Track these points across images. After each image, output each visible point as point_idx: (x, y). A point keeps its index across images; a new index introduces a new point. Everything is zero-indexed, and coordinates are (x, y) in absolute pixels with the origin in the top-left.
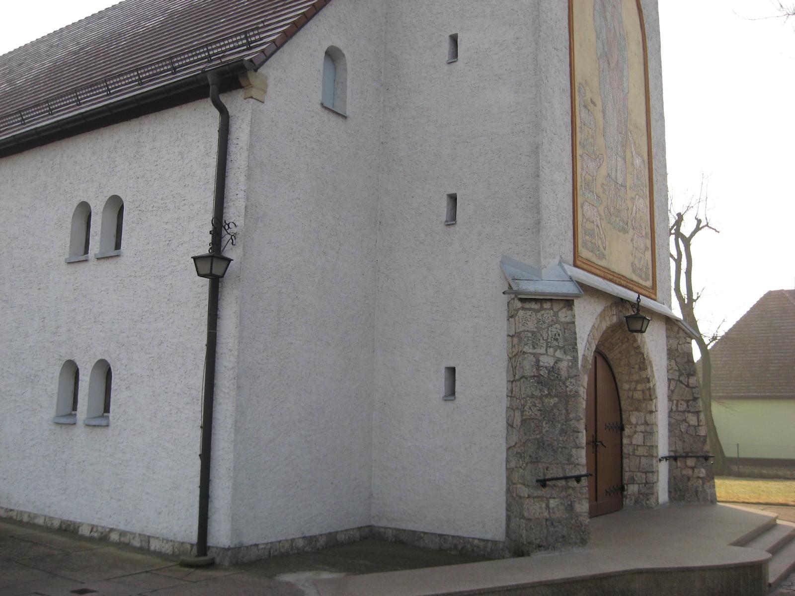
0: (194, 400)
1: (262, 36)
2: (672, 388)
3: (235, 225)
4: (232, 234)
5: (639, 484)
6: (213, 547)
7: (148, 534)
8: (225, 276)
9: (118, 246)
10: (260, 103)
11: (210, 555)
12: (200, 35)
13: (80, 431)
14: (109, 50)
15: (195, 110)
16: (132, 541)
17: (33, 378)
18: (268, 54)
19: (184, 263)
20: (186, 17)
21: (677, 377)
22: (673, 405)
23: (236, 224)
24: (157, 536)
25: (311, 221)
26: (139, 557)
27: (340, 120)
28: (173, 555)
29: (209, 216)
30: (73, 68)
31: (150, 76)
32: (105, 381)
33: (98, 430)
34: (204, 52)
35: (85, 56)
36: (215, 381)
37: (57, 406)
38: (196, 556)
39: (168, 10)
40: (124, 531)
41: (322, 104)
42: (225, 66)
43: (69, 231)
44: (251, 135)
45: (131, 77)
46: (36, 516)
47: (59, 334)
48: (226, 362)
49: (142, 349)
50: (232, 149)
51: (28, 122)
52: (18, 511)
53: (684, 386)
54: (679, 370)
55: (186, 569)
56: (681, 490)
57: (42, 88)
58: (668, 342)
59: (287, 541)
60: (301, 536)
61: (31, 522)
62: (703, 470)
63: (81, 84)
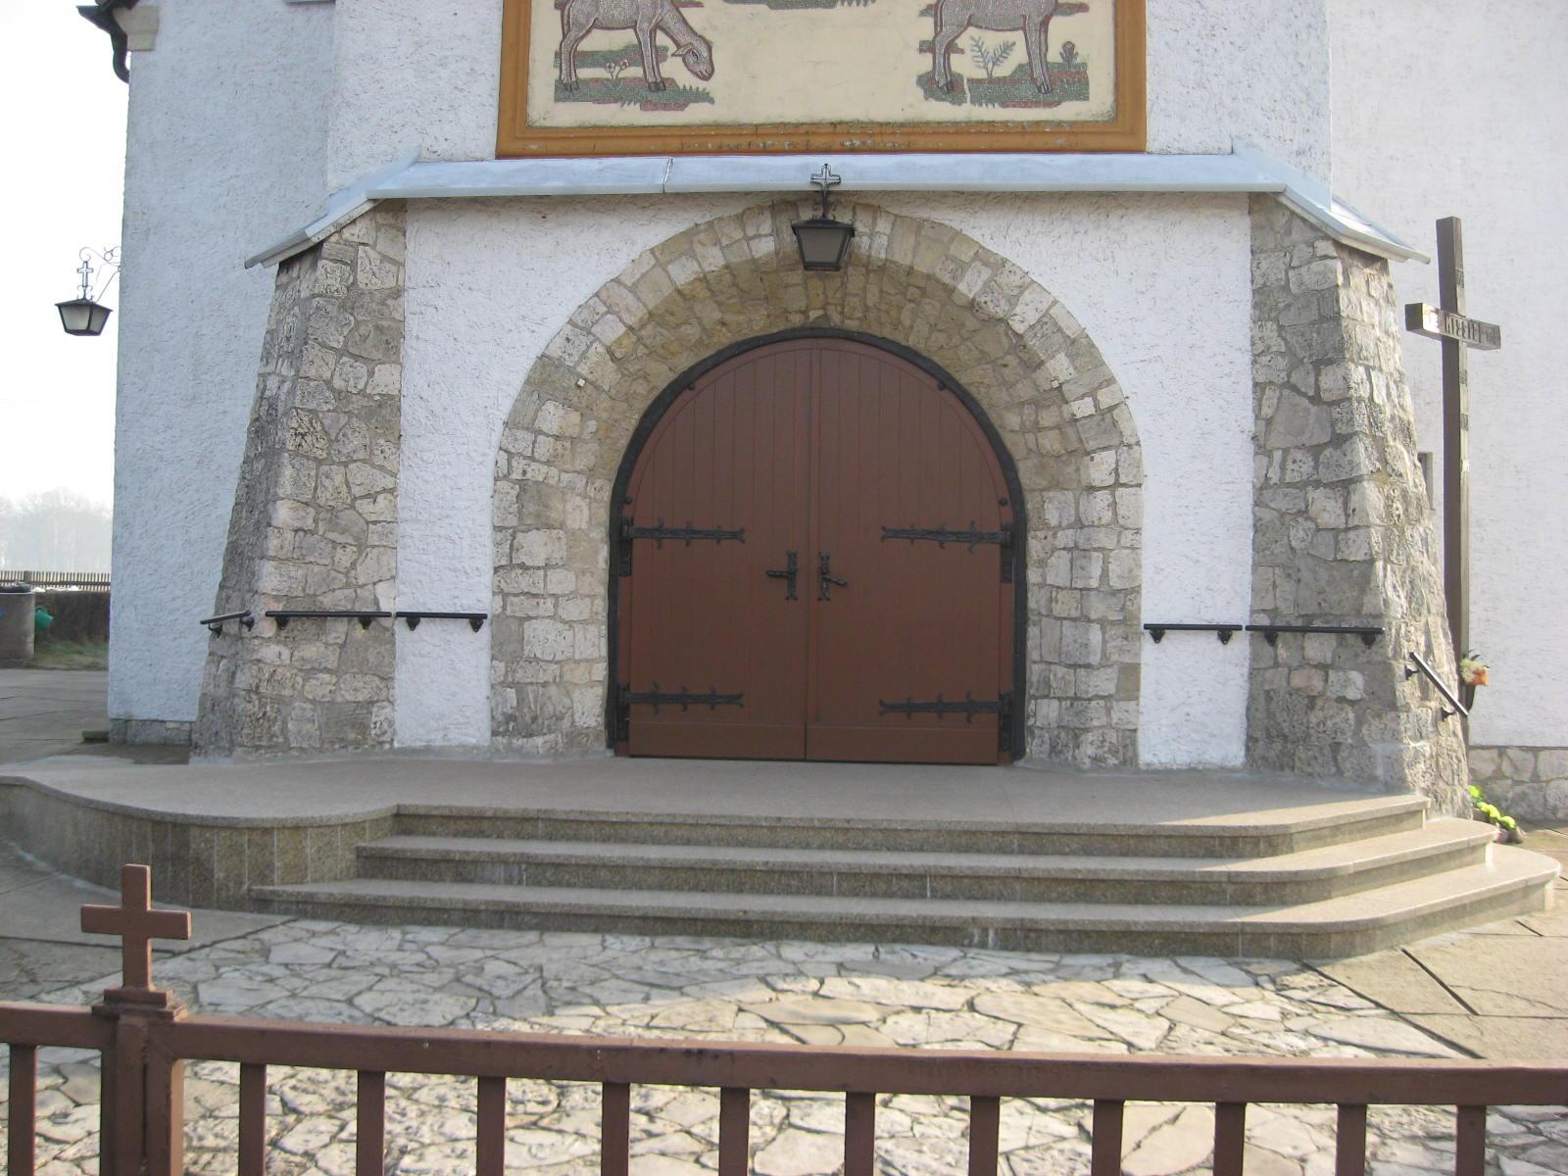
2: (1267, 411)
5: (1060, 699)
21: (1283, 374)
22: (1270, 463)
53: (1305, 402)
54: (1290, 352)
56: (1285, 738)
58: (1256, 265)
62: (1357, 677)
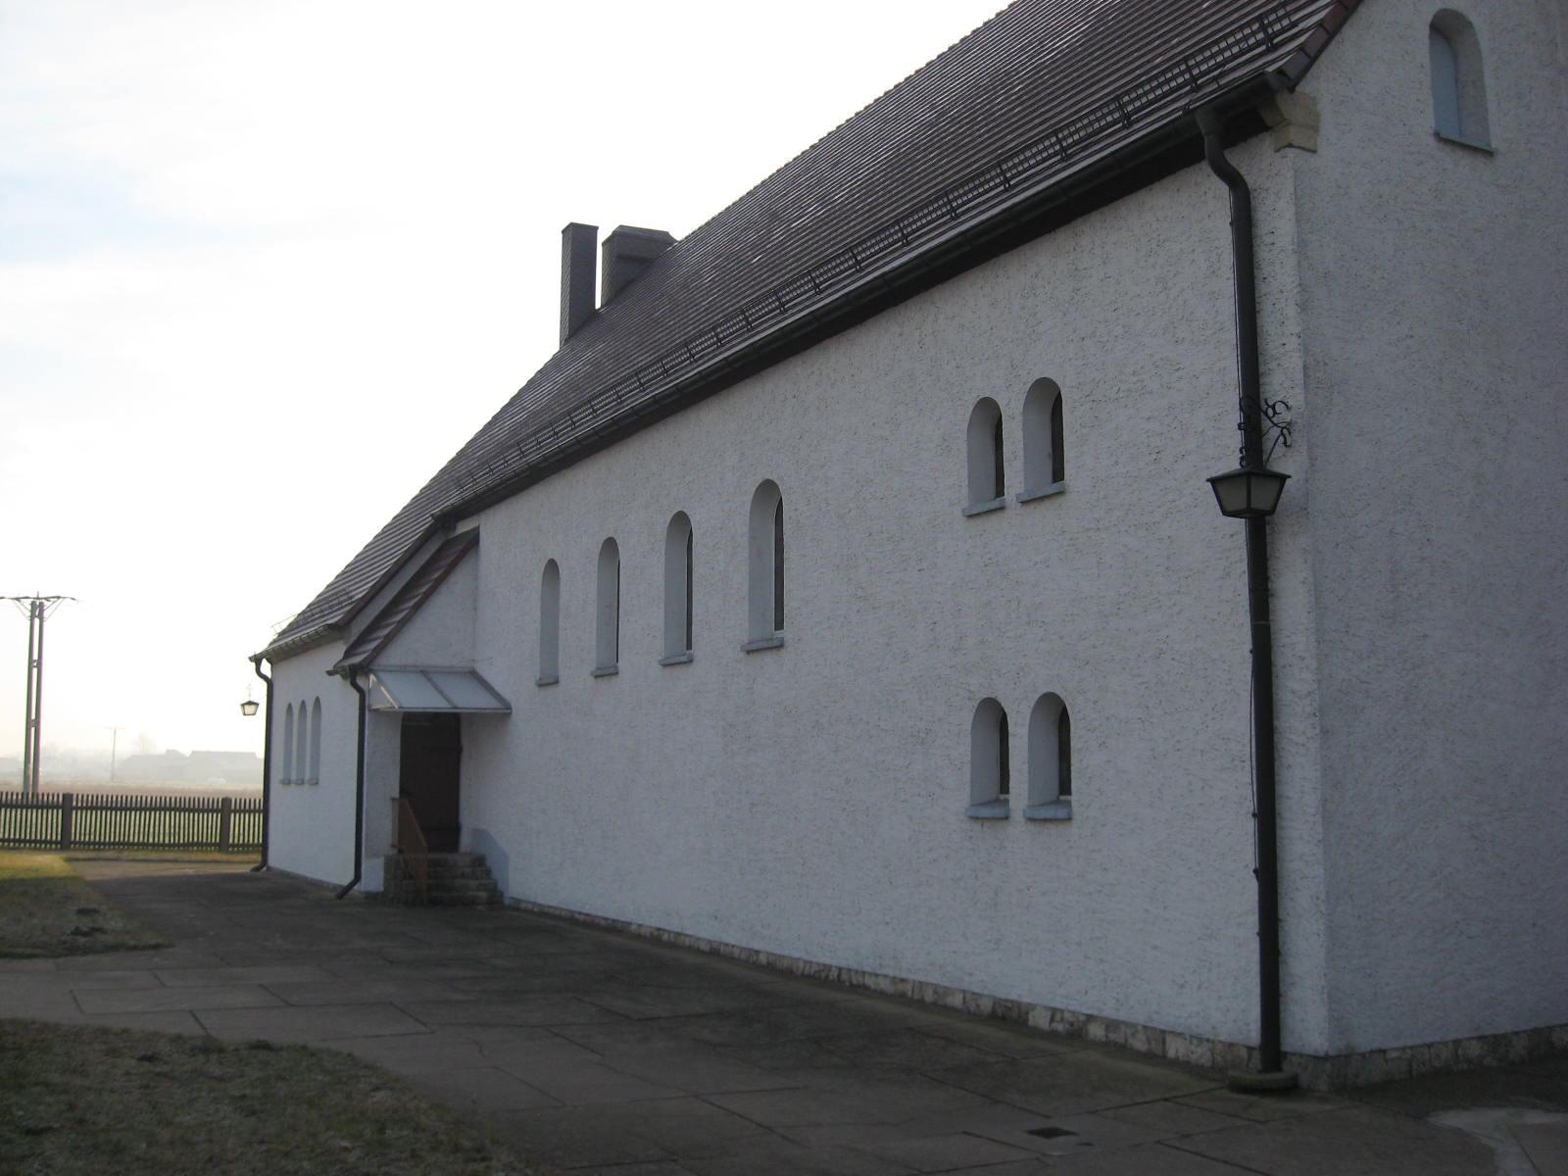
0: (1236, 763)
1: (1294, 18)
3: (1287, 406)
4: (1284, 425)
6: (1294, 1054)
7: (1162, 1027)
8: (1278, 509)
9: (1058, 474)
10: (1309, 154)
11: (1288, 1069)
12: (1165, 42)
13: (1017, 829)
14: (993, 107)
15: (1178, 190)
16: (1130, 1040)
17: (922, 735)
18: (1312, 53)
19: (1191, 494)
20: (1129, 15)
23: (1289, 404)
24: (1180, 1030)
25: (1441, 380)
26: (1147, 1070)
27: (1480, 161)
28: (1212, 1067)
29: (1232, 397)
30: (931, 153)
31: (1081, 140)
32: (1056, 731)
33: (1052, 829)
34: (1182, 73)
35: (951, 127)
36: (1275, 723)
37: (972, 787)
38: (1260, 1072)
39: (1094, 8)
40: (1114, 1020)
41: (1437, 135)
42: (1227, 92)
43: (964, 456)
44: (1298, 221)
45: (1046, 149)
46: (947, 991)
47: (964, 652)
48: (1295, 683)
49: (1124, 669)
50: (1264, 254)
51: (868, 266)
52: (914, 981)
55: (1244, 1097)
57: (881, 200)
59: (1445, 1044)
60: (1474, 1034)
61: (940, 1002)
63: (952, 180)
